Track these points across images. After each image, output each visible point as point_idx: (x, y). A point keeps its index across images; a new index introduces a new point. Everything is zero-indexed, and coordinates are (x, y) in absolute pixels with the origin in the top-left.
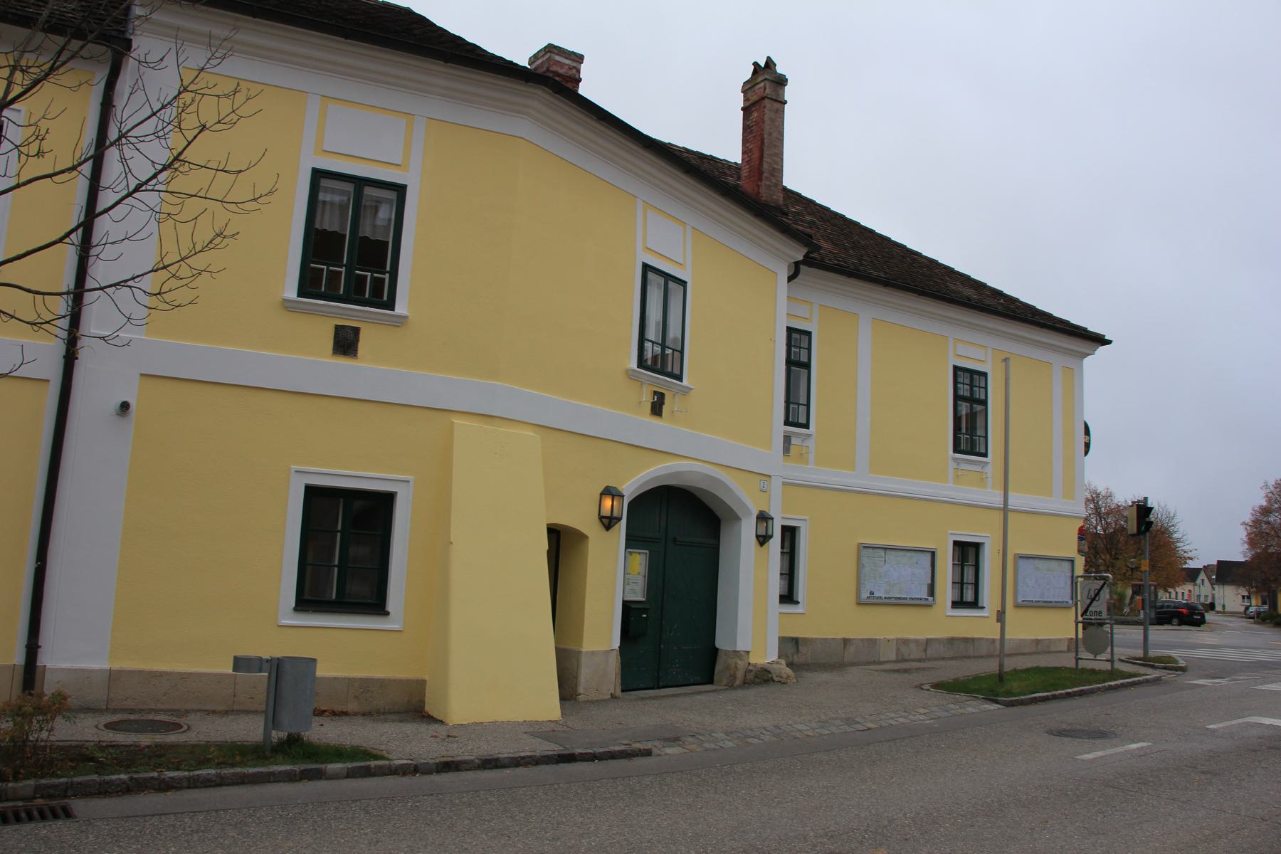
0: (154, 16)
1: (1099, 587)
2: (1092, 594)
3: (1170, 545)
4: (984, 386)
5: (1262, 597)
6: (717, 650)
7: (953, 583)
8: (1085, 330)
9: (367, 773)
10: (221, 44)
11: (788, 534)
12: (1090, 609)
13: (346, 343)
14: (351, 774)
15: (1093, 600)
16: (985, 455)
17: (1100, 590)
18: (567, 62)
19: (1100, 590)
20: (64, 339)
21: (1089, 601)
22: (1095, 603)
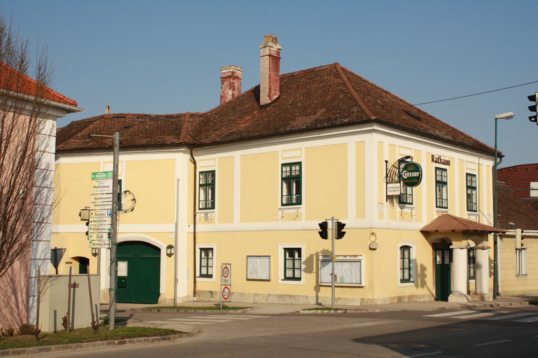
5: (204, 188)
7: (212, 267)
18: (227, 71)
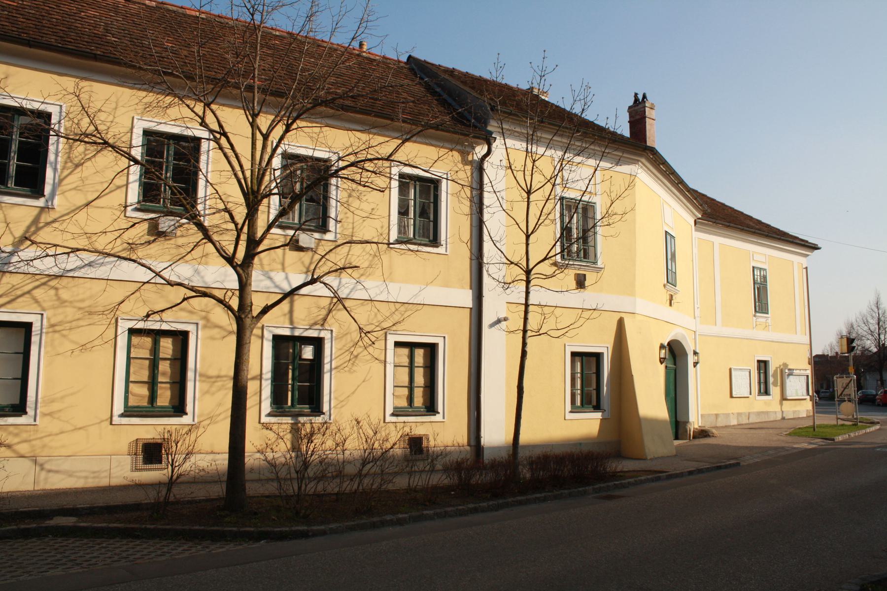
0: (554, 138)
1: (848, 382)
2: (844, 385)
3: (856, 356)
4: (593, 245)
6: (679, 422)
8: (59, 75)
9: (658, 479)
10: (619, 160)
11: (762, 365)
12: (844, 393)
13: (581, 283)
14: (652, 480)
15: (845, 388)
16: (767, 313)
17: (849, 383)
19: (849, 383)
20: (15, 238)
21: (843, 389)
22: (846, 390)
